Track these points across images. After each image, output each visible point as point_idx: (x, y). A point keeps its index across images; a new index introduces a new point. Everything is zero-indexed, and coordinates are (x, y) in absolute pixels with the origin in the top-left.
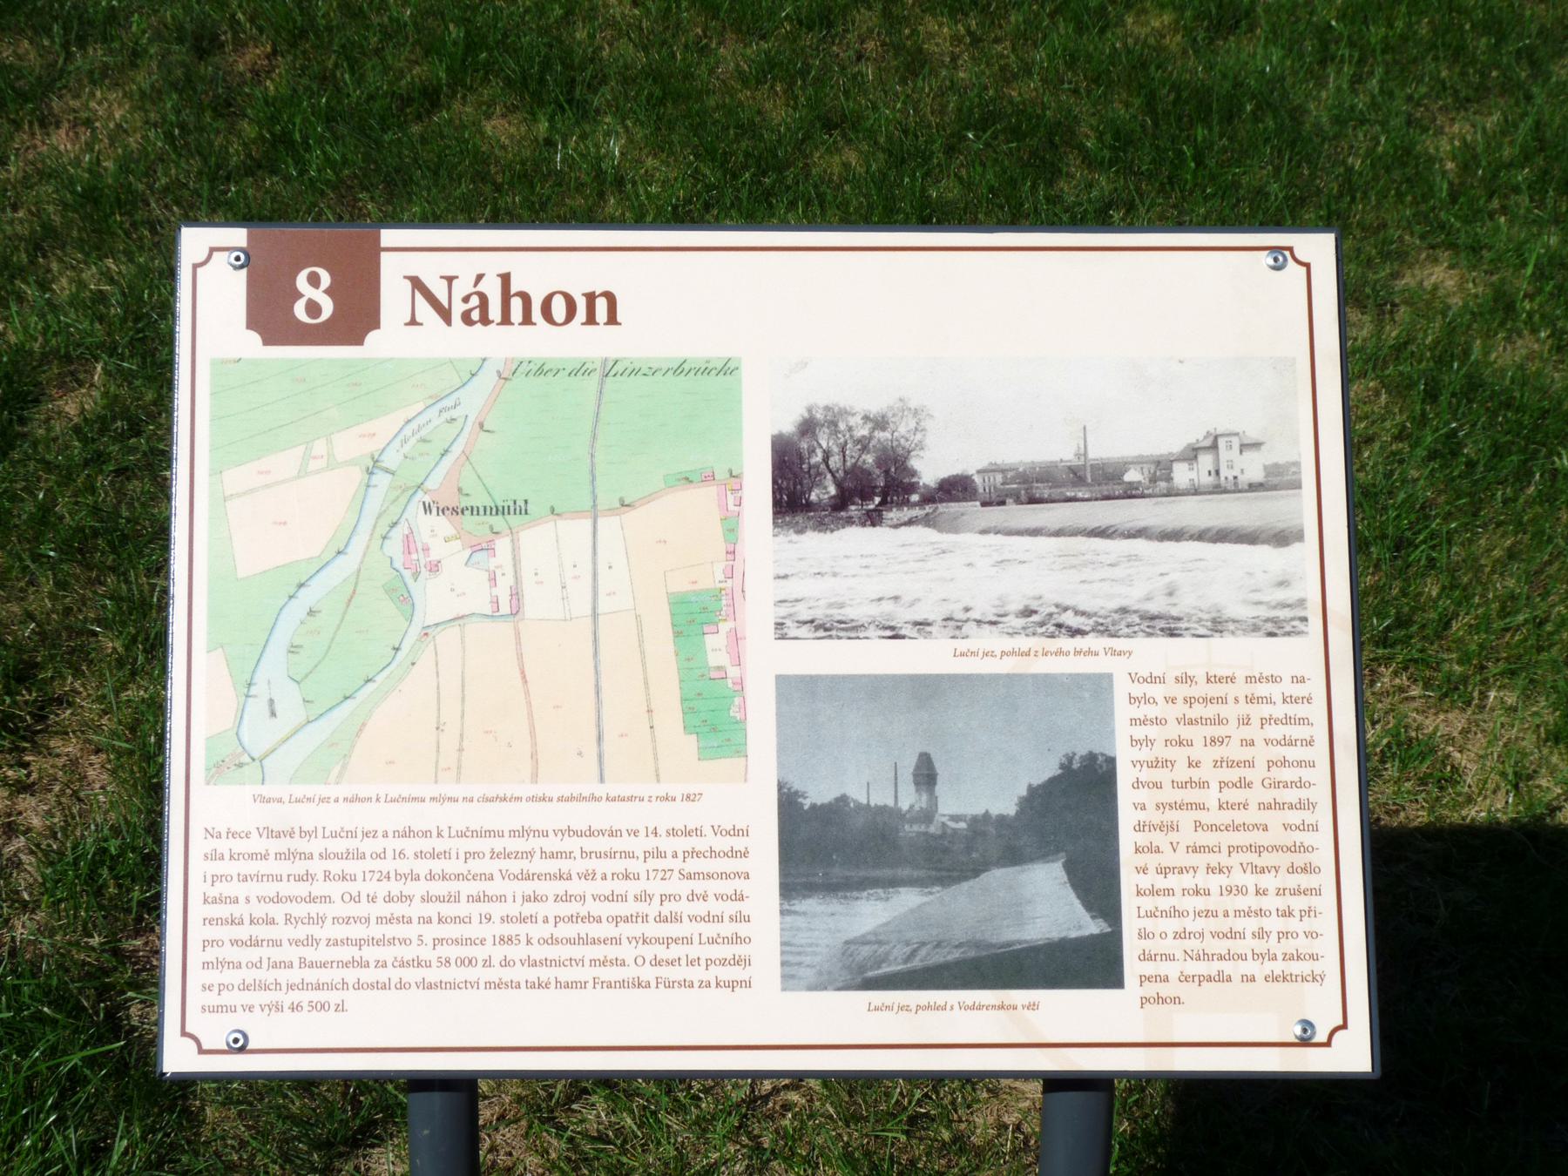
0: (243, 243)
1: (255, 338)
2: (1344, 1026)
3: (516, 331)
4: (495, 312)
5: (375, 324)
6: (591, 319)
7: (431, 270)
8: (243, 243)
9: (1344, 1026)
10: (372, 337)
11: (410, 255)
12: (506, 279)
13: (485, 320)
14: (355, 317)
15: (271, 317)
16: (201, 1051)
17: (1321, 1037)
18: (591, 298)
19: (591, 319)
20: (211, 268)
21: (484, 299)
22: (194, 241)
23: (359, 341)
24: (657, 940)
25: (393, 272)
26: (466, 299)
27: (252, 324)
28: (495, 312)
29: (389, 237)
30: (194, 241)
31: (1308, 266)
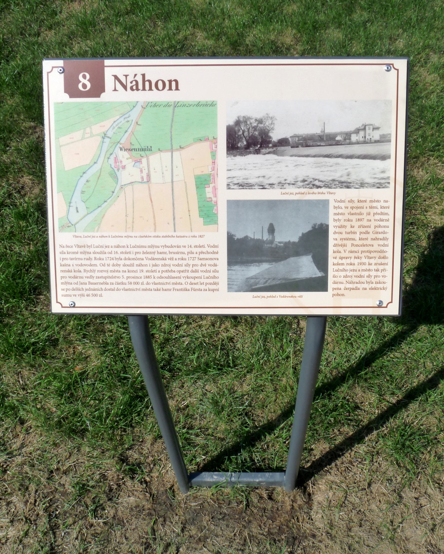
0: (62, 65)
1: (67, 95)
2: (392, 302)
3: (147, 93)
4: (140, 87)
5: (104, 91)
6: (170, 89)
7: (120, 73)
8: (62, 65)
9: (392, 302)
10: (103, 95)
11: (113, 68)
12: (144, 75)
13: (137, 89)
14: (98, 89)
15: (72, 89)
16: (62, 307)
17: (384, 305)
18: (170, 82)
19: (170, 89)
20: (53, 73)
21: (137, 82)
22: (48, 65)
23: (99, 96)
24: (191, 277)
25: (109, 73)
26: (131, 82)
27: (66, 91)
28: (140, 87)
29: (107, 62)
30: (48, 65)
31: (398, 70)
